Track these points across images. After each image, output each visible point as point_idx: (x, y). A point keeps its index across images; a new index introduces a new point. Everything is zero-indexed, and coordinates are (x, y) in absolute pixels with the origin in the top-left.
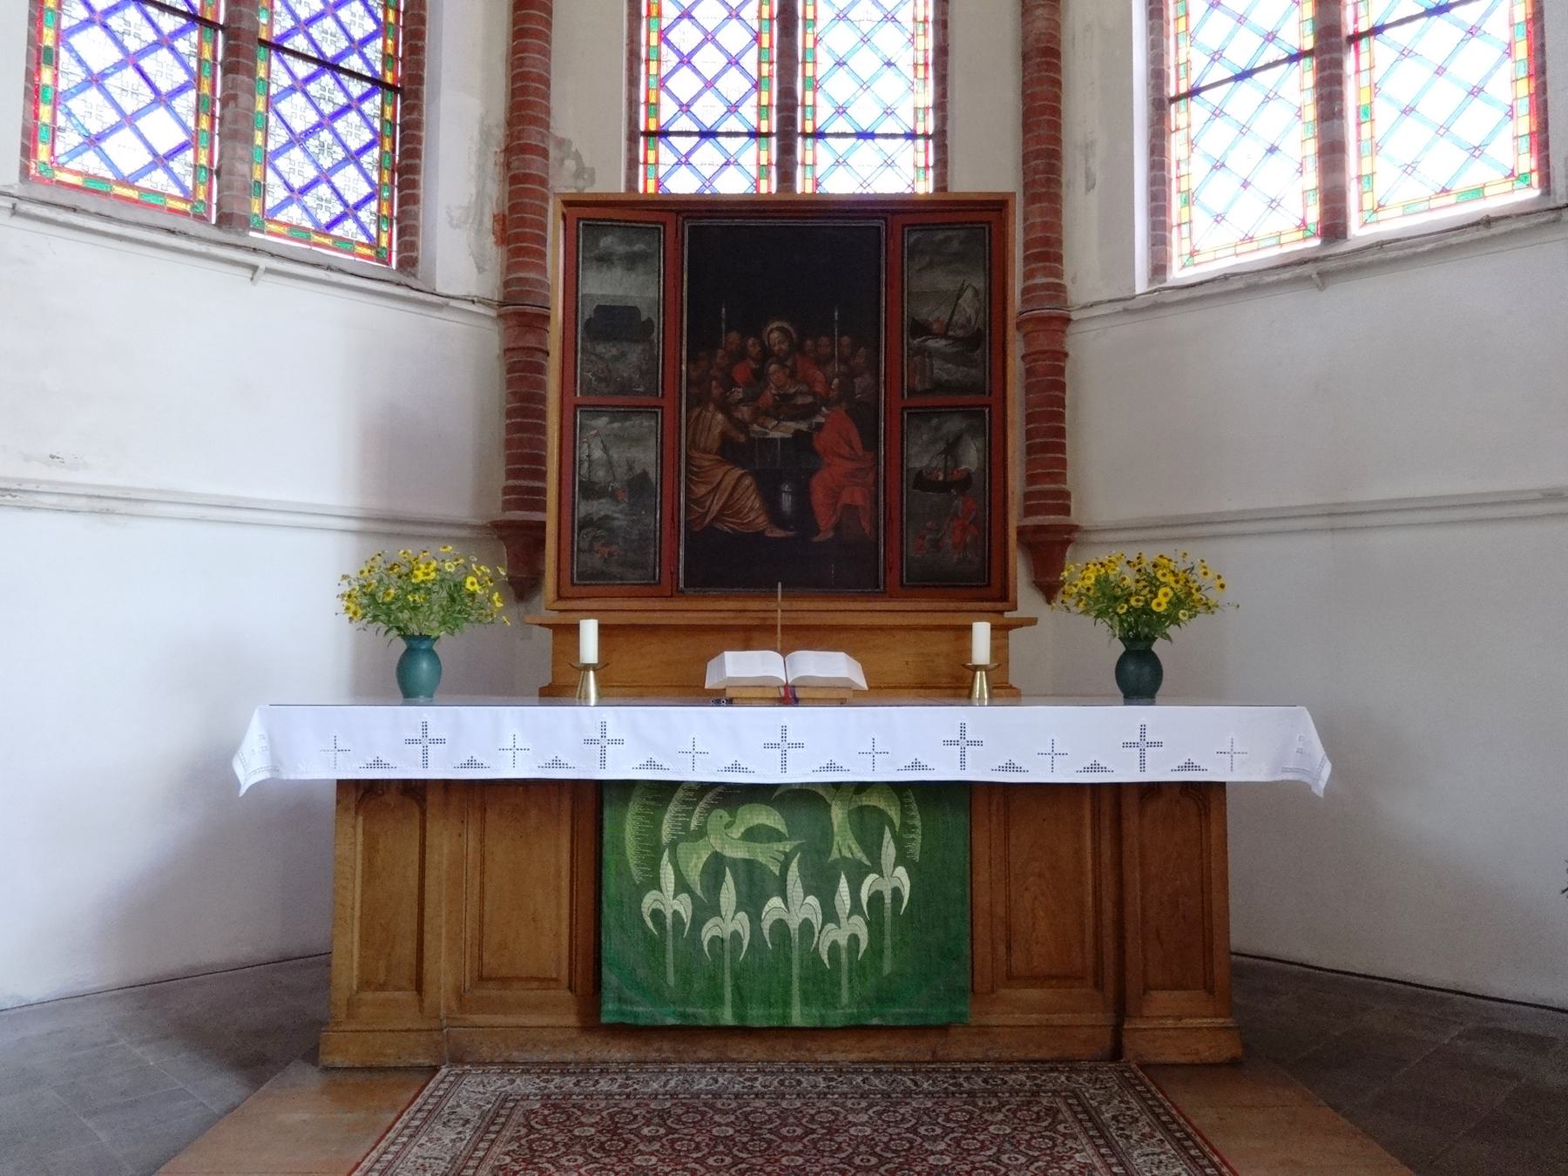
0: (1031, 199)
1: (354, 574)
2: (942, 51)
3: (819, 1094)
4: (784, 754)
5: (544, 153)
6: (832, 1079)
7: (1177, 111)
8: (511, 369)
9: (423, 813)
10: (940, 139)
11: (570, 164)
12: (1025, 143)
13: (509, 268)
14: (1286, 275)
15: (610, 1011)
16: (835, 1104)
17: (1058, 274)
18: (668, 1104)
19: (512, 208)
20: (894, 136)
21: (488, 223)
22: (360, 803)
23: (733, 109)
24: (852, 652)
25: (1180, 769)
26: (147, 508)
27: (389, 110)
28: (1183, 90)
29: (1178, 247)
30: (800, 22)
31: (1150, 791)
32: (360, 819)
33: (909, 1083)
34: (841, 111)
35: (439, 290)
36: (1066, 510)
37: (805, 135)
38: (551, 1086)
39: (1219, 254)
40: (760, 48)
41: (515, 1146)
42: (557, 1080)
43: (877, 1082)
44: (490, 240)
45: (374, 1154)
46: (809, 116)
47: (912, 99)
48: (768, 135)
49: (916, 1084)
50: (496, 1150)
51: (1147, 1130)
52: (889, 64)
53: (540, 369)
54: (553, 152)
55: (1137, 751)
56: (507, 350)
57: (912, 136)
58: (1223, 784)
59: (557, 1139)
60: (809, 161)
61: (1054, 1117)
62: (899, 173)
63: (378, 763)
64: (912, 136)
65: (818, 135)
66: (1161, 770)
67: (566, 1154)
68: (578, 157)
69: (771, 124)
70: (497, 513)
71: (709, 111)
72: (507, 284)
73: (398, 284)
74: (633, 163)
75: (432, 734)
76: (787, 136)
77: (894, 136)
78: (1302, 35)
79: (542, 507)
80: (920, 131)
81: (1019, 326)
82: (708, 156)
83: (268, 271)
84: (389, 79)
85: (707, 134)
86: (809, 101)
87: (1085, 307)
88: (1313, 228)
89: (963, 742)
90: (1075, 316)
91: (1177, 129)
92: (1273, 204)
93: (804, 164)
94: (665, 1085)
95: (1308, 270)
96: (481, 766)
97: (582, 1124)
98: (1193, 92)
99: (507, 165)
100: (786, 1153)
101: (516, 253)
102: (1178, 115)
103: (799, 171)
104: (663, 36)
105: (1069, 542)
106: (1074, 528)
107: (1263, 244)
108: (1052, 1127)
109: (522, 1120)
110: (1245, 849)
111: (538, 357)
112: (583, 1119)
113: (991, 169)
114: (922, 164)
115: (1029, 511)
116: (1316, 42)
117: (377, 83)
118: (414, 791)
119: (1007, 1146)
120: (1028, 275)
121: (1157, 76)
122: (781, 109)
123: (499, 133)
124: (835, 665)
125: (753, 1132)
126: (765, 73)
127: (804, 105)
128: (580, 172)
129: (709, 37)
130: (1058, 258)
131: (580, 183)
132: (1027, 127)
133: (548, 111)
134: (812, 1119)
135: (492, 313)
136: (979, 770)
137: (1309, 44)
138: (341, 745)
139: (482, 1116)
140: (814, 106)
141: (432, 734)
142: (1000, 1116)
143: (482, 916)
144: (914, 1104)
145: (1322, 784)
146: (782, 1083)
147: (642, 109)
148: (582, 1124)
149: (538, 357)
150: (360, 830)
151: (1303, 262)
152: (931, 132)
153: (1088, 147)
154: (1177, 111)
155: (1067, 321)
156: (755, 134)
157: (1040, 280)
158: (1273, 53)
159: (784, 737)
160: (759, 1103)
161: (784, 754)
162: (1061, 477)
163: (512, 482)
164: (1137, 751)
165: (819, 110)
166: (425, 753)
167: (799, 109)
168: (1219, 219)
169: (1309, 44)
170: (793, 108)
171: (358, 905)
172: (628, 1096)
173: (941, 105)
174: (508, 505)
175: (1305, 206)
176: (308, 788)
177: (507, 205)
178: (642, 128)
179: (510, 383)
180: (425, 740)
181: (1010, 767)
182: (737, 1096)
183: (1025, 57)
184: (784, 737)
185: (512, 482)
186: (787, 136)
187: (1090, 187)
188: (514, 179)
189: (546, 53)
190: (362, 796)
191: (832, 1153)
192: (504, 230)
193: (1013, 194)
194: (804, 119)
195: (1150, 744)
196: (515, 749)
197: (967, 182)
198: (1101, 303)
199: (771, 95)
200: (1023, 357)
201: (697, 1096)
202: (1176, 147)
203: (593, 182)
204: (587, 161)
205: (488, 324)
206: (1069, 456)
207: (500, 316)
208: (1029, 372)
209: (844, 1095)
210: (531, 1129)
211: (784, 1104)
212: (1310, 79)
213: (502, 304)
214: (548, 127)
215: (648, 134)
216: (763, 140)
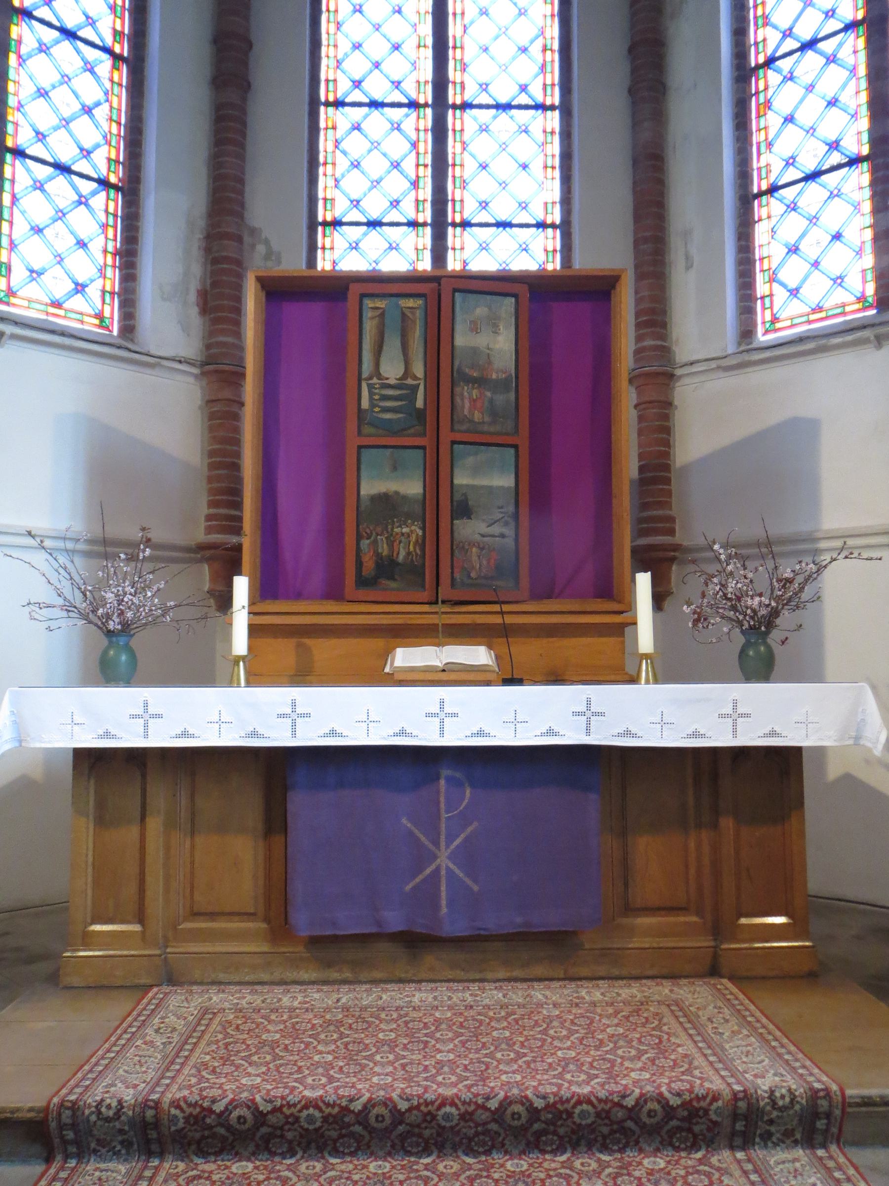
0: (640, 276)
1: (45, 594)
2: (566, 157)
3: (466, 1007)
4: (442, 722)
5: (239, 239)
6: (476, 996)
7: (760, 206)
8: (212, 416)
9: (144, 776)
10: (565, 227)
11: (261, 249)
12: (636, 232)
13: (211, 334)
14: (849, 338)
15: (303, 922)
16: (480, 1014)
17: (663, 337)
18: (340, 1016)
19: (214, 284)
20: (527, 226)
21: (193, 297)
22: (92, 768)
23: (395, 203)
24: (490, 647)
25: (765, 736)
26: (694, 369)
27: (111, 205)
28: (764, 187)
29: (762, 316)
30: (450, 133)
31: (740, 755)
32: (92, 782)
33: (540, 997)
34: (484, 205)
35: (153, 352)
36: (671, 532)
37: (454, 225)
38: (244, 1002)
39: (796, 321)
40: (418, 153)
41: (214, 1047)
42: (249, 998)
43: (514, 997)
44: (194, 311)
45: (107, 1045)
46: (458, 208)
47: (544, 193)
48: (425, 224)
49: (546, 997)
50: (198, 1051)
51: (736, 1028)
52: (524, 167)
53: (237, 417)
54: (247, 239)
55: (730, 720)
56: (210, 402)
57: (542, 225)
58: (799, 750)
59: (249, 1042)
60: (458, 246)
61: (660, 1020)
62: (533, 253)
63: (107, 735)
64: (542, 225)
65: (465, 224)
66: (751, 736)
67: (256, 1053)
68: (267, 242)
69: (426, 215)
70: (200, 536)
71: (375, 208)
72: (208, 347)
73: (119, 347)
74: (312, 248)
75: (151, 710)
76: (440, 226)
77: (527, 226)
78: (859, 142)
79: (238, 531)
80: (549, 221)
81: (631, 381)
82: (374, 241)
83: (14, 337)
84: (113, 179)
85: (374, 224)
86: (458, 197)
87: (461, 118)
88: (870, 300)
89: (589, 714)
90: (678, 372)
91: (760, 220)
92: (839, 281)
93: (454, 249)
94: (338, 1001)
95: (867, 333)
96: (193, 736)
97: (268, 1031)
98: (773, 189)
99: (208, 250)
100: (439, 1051)
101: (215, 321)
102: (760, 210)
103: (450, 253)
104: (337, 143)
105: (673, 560)
106: (676, 548)
107: (830, 313)
108: (659, 1028)
109: (219, 1028)
110: (817, 813)
111: (235, 408)
112: (269, 1027)
113: (608, 251)
114: (458, 168)
115: (641, 533)
116: (871, 149)
117: (104, 183)
118: (137, 760)
119: (621, 1043)
120: (639, 338)
121: (744, 174)
122: (434, 203)
123: (201, 223)
124: (479, 655)
125: (410, 1034)
126: (421, 174)
127: (453, 200)
128: (268, 256)
129: (375, 145)
130: (664, 325)
131: (269, 264)
132: (637, 218)
133: (242, 205)
134: (461, 1025)
135: (196, 371)
136: (602, 736)
137: (865, 150)
138: (77, 719)
139: (187, 1025)
140: (462, 201)
141: (151, 710)
142: (616, 1021)
143: (192, 863)
144: (509, 1165)
145: (880, 747)
146: (435, 998)
147: (320, 204)
148: (268, 1031)
149: (235, 408)
150: (92, 792)
151: (864, 327)
152: (558, 222)
153: (687, 234)
154: (760, 206)
155: (671, 376)
156: (413, 224)
157: (648, 342)
158: (836, 158)
159: (442, 708)
160: (415, 1014)
161: (442, 722)
162: (667, 505)
163: (212, 511)
164: (730, 720)
165: (466, 202)
166: (146, 726)
167: (450, 204)
168: (794, 292)
169: (865, 150)
170: (445, 202)
171: (90, 853)
172: (307, 1010)
173: (566, 201)
174: (209, 530)
175: (864, 281)
176: (52, 754)
177: (209, 282)
178: (320, 219)
179: (211, 429)
180: (147, 715)
181: (628, 733)
182: (398, 1009)
183: (635, 162)
184: (442, 708)
185: (212, 511)
186: (440, 226)
187: (689, 267)
188: (215, 261)
189: (242, 157)
190: (92, 763)
191: (478, 1051)
192: (205, 302)
193: (623, 270)
194: (454, 211)
195: (741, 715)
196: (220, 722)
197: (586, 262)
198: (698, 361)
199: (426, 192)
200: (636, 406)
201: (363, 1009)
202: (761, 233)
203: (279, 263)
204: (275, 246)
205: (191, 380)
206: (674, 486)
207: (203, 374)
208: (641, 418)
209: (488, 1007)
210: (227, 1035)
211: (437, 1015)
212: (866, 179)
213: (204, 364)
214: (241, 216)
215: (325, 224)
216: (420, 228)
